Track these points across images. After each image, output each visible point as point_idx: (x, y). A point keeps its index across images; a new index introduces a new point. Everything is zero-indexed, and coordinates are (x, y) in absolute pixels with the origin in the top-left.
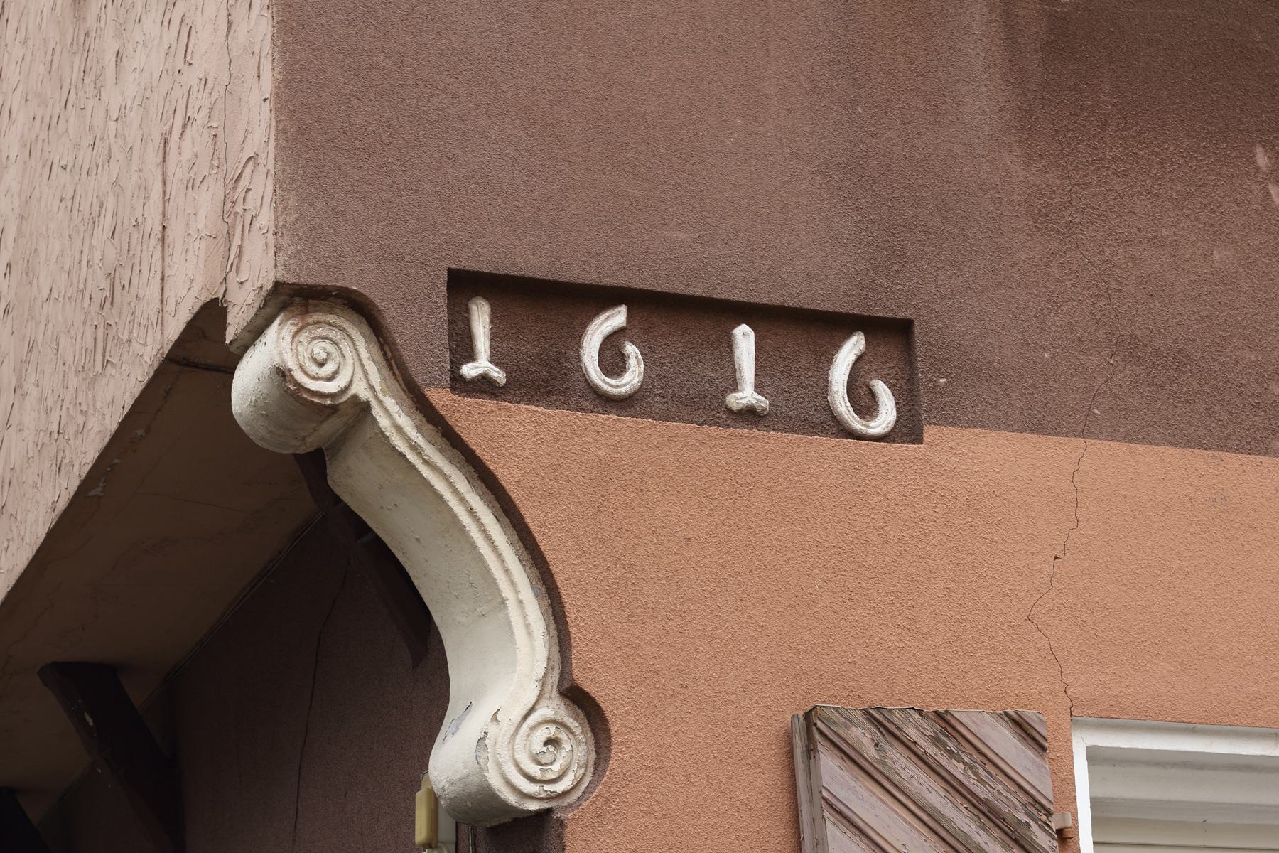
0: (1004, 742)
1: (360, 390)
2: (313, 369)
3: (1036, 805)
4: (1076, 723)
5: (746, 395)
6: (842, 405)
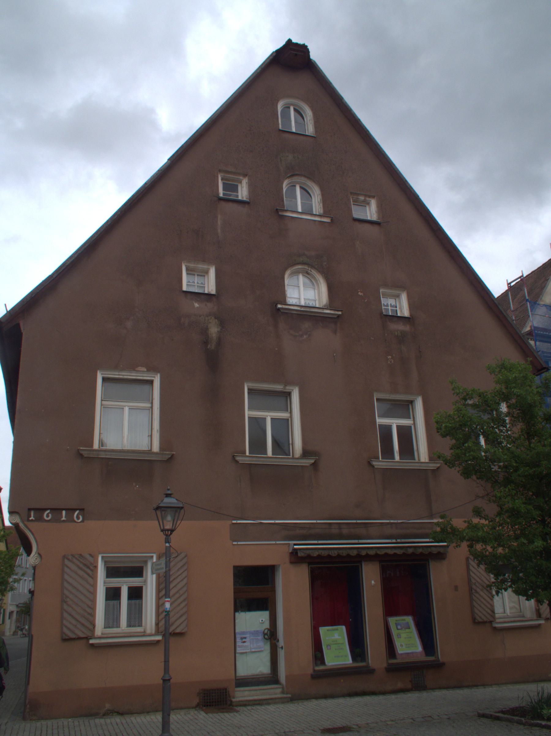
0: (88, 557)
1: (18, 522)
2: (12, 520)
3: (91, 564)
4: (99, 553)
5: (64, 518)
6: (75, 519)
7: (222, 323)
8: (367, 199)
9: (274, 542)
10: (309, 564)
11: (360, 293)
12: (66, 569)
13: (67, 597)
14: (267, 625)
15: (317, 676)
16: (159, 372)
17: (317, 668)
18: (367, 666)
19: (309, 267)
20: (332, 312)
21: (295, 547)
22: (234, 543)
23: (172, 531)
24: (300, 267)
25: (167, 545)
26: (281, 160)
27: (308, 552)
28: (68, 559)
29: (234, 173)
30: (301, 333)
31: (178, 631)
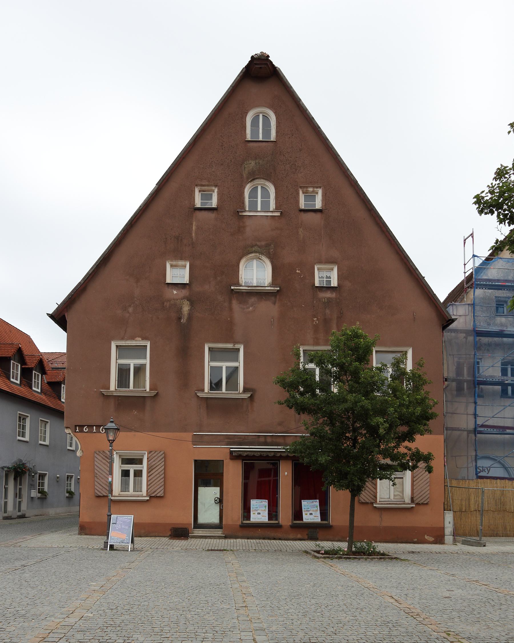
6: (101, 431)
7: (192, 304)
8: (315, 189)
9: (220, 447)
10: (243, 460)
11: (297, 271)
12: (96, 459)
13: (97, 474)
14: (218, 496)
15: (243, 526)
16: (149, 340)
17: (245, 522)
18: (278, 523)
19: (260, 254)
20: (272, 288)
21: (231, 449)
22: (194, 446)
23: (114, 441)
24: (253, 255)
25: (110, 448)
26: (245, 168)
27: (240, 453)
28: (97, 454)
29: (208, 185)
30: (248, 306)
31: (158, 495)
